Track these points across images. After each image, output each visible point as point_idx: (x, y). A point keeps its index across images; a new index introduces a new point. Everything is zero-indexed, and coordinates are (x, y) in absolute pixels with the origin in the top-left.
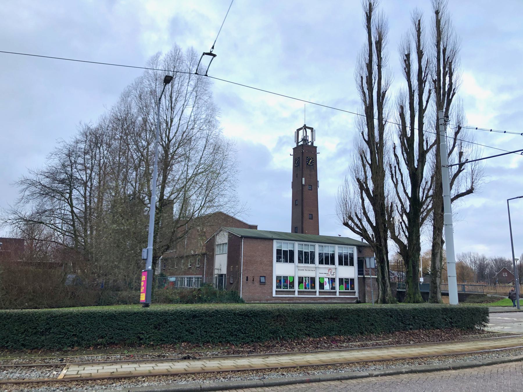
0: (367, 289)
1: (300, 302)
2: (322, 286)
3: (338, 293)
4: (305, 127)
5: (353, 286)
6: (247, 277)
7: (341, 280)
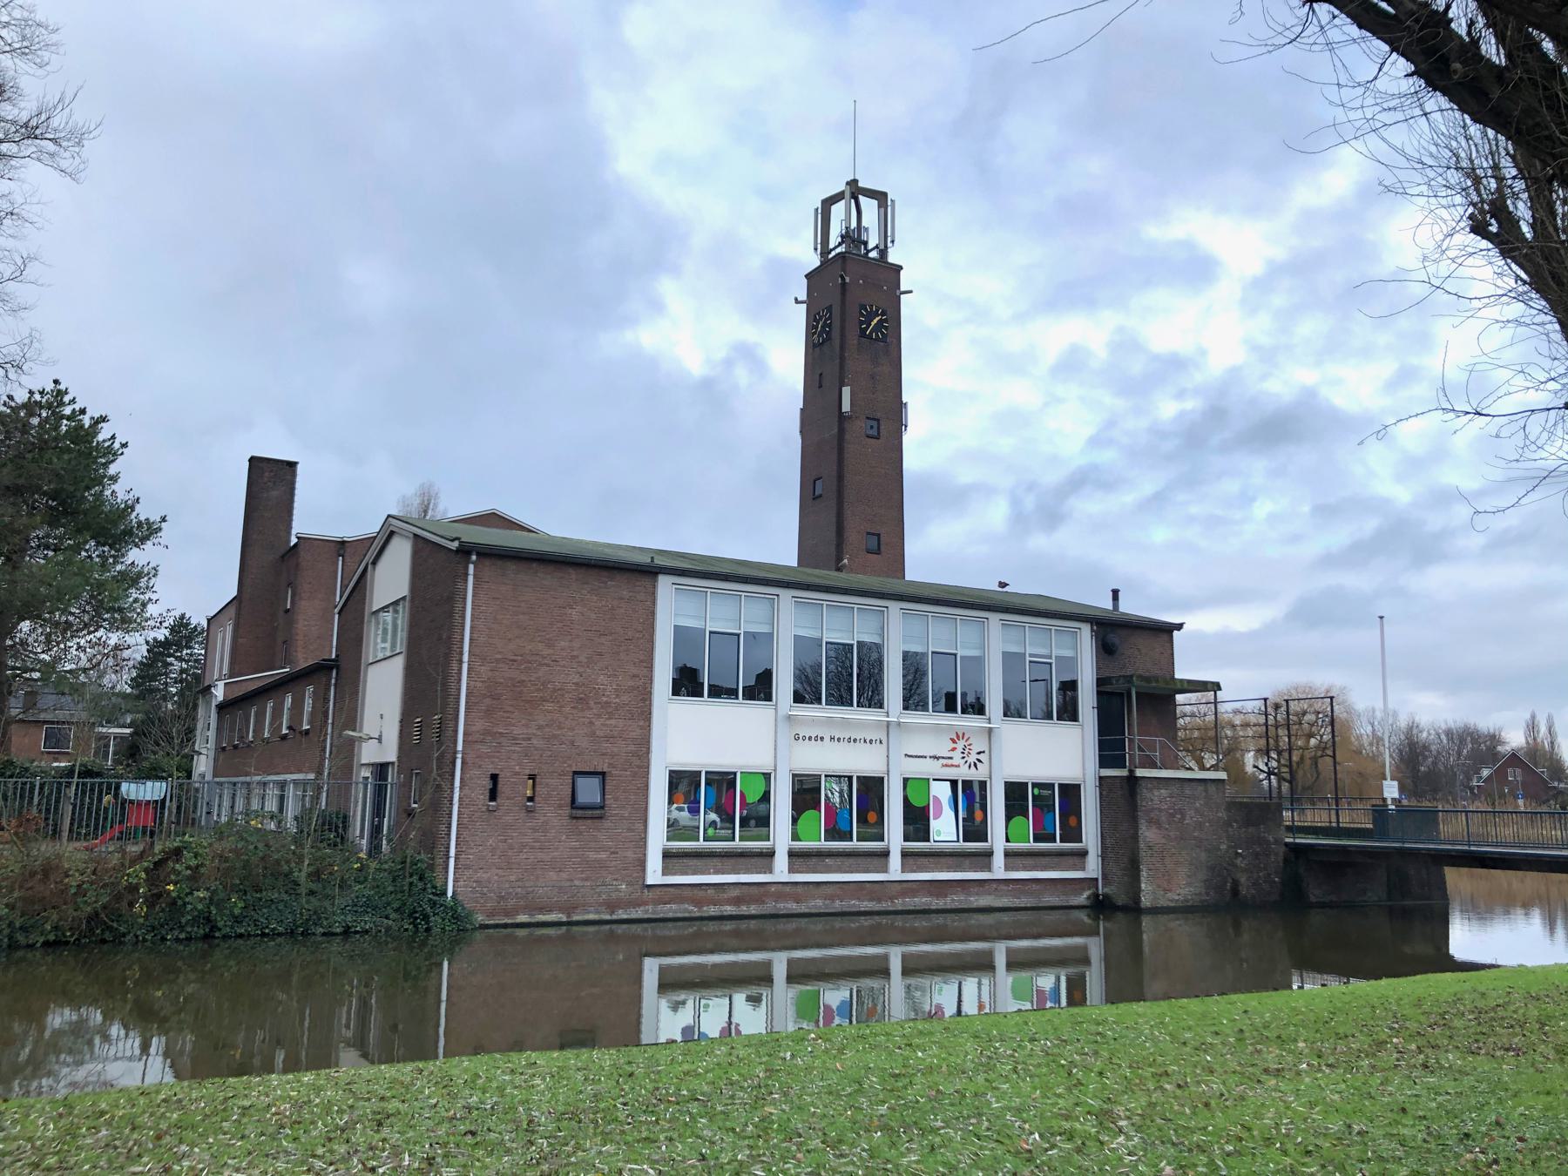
0: (1148, 834)
1: (803, 909)
2: (917, 820)
3: (999, 860)
4: (855, 191)
5: (1072, 821)
6: (494, 778)
7: (1015, 793)
